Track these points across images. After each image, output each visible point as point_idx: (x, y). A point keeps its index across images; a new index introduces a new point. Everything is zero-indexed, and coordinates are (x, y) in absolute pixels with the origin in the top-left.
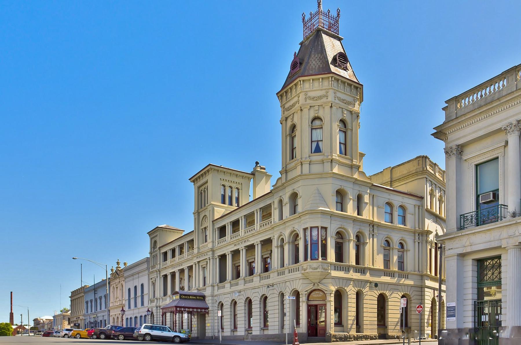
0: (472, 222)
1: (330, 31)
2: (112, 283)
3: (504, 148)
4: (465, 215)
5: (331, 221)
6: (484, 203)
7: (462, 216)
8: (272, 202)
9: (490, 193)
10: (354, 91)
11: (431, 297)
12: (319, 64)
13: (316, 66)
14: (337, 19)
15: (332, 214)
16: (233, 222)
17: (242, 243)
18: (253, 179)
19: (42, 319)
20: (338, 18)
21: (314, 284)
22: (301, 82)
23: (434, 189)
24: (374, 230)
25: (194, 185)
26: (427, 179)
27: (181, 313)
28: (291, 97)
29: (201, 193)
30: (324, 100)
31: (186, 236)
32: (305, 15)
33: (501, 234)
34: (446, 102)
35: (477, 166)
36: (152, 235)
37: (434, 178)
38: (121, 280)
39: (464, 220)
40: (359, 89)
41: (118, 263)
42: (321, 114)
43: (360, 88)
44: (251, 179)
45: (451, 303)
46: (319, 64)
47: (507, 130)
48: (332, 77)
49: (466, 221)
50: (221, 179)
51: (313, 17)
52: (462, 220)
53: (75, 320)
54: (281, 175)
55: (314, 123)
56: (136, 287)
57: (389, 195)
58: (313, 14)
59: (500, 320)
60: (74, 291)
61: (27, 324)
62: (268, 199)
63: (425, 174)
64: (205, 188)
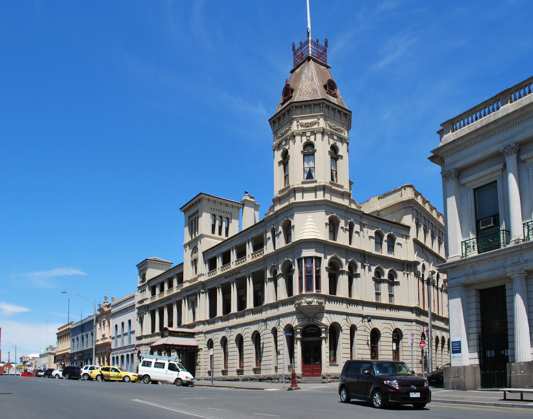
0: (474, 249)
1: (319, 59)
2: (99, 318)
3: (502, 171)
5: (325, 251)
6: (484, 229)
7: (463, 243)
8: (231, 248)
9: (491, 218)
10: (343, 118)
11: (421, 332)
12: (310, 91)
13: (307, 92)
14: (325, 48)
15: (326, 244)
16: (161, 283)
17: (233, 275)
18: (242, 208)
19: (29, 357)
20: (325, 47)
21: (309, 319)
22: (293, 108)
23: (419, 217)
24: (366, 260)
25: (185, 214)
26: (413, 208)
27: (169, 352)
28: (283, 123)
29: (192, 223)
30: (316, 126)
31: (175, 269)
32: (295, 45)
33: (505, 261)
34: (441, 125)
35: (475, 190)
36: (141, 268)
37: (419, 207)
38: (109, 316)
40: (348, 116)
41: (106, 298)
42: (312, 139)
43: (349, 115)
44: (240, 209)
45: (456, 338)
46: (310, 91)
47: (505, 152)
49: (531, 230)
50: (211, 208)
51: (303, 45)
52: (464, 247)
53: (61, 359)
54: (274, 203)
55: (306, 149)
56: (123, 323)
57: (379, 224)
58: (302, 43)
59: (506, 355)
60: (62, 326)
61: (14, 362)
62: (260, 228)
63: (411, 203)
64: (195, 218)
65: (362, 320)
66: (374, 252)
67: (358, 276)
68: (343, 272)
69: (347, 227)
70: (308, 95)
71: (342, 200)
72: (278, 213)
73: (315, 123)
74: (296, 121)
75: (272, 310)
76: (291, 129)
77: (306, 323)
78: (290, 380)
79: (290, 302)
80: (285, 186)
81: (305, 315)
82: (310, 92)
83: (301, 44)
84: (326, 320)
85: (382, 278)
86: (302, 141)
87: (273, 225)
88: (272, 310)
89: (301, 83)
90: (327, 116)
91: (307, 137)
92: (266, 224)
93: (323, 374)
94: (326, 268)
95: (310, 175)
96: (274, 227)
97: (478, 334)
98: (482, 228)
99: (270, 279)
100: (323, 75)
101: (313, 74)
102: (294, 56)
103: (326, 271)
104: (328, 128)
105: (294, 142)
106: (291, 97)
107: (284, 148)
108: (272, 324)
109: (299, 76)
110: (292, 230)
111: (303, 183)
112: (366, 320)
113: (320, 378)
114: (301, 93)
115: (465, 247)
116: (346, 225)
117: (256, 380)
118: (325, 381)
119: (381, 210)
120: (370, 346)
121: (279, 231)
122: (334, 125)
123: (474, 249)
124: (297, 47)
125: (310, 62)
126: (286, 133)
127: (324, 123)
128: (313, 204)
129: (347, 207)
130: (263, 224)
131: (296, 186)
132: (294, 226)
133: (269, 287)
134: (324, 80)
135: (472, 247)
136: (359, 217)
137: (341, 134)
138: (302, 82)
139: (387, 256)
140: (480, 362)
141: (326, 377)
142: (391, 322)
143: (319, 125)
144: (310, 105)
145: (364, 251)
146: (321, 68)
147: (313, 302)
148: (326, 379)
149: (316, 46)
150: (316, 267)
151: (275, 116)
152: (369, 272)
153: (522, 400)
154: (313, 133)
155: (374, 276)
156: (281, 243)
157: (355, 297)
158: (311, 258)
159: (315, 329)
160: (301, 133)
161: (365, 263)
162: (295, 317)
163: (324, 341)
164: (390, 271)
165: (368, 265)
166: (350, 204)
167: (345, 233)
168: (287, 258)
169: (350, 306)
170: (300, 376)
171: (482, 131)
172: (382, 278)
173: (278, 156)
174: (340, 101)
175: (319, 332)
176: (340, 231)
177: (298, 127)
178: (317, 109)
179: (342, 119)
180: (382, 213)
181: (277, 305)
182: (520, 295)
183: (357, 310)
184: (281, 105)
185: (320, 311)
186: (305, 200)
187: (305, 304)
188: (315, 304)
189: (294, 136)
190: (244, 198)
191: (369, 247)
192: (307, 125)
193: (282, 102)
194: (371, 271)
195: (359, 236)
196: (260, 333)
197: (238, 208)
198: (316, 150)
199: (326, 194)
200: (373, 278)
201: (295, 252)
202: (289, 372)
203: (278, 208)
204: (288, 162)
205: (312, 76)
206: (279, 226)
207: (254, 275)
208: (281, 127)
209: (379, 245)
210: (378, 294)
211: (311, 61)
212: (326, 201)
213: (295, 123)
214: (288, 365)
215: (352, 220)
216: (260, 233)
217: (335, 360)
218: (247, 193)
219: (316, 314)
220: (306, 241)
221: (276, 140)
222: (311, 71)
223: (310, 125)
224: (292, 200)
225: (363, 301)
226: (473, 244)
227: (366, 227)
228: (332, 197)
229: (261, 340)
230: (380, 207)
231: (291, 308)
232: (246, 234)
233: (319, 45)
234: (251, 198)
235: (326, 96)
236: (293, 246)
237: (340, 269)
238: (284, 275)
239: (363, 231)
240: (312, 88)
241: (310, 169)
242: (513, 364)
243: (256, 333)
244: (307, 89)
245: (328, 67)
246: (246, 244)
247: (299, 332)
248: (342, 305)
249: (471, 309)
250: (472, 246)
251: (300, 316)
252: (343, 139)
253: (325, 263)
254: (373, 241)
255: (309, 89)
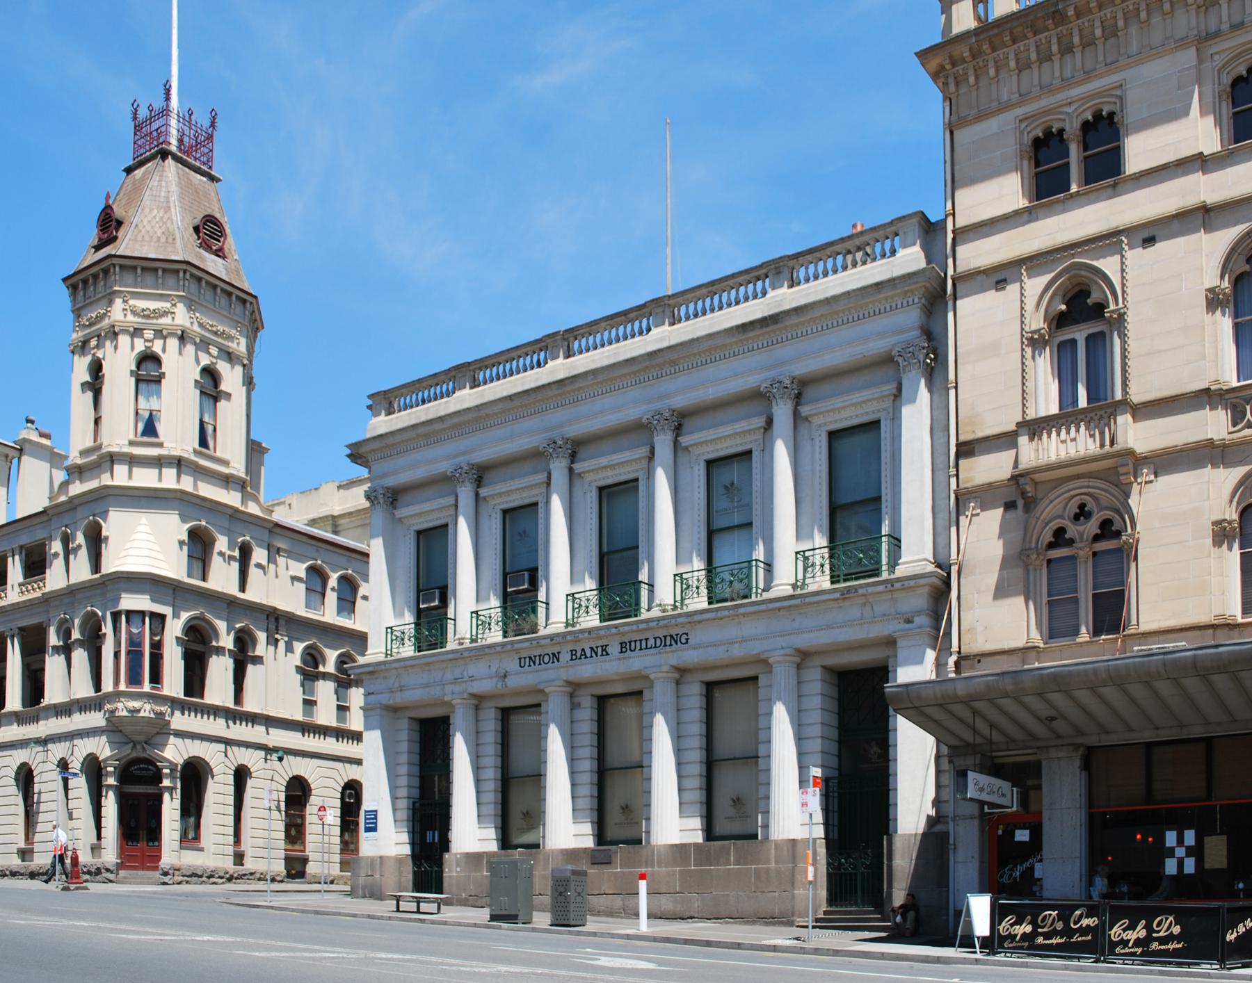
0: (823, 572)
4: (576, 596)
10: (238, 308)
13: (152, 237)
30: (166, 320)
35: (505, 512)
39: (573, 607)
42: (157, 347)
43: (251, 303)
46: (159, 235)
48: (185, 271)
52: (800, 564)
55: (143, 365)
57: (318, 551)
65: (266, 756)
66: (302, 612)
67: (258, 660)
68: (220, 651)
69: (234, 551)
70: (153, 244)
71: (226, 491)
72: (76, 502)
73: (166, 313)
74: (121, 300)
75: (59, 717)
76: (109, 314)
77: (128, 755)
78: (91, 875)
79: (95, 705)
80: (95, 442)
81: (126, 736)
82: (159, 238)
83: (151, 111)
84: (174, 752)
85: (321, 669)
86: (133, 348)
87: (66, 526)
88: (59, 717)
89: (139, 210)
90: (196, 302)
91: (146, 341)
92: (50, 520)
93: (162, 866)
94: (177, 638)
95: (150, 429)
96: (67, 533)
97: (411, 800)
98: (425, 606)
99: (57, 649)
100: (198, 199)
101: (171, 194)
102: (135, 134)
103: (178, 645)
104: (196, 328)
105: (116, 347)
106: (115, 238)
107: (94, 355)
108: (58, 751)
109: (139, 188)
110: (103, 545)
111: (131, 443)
112: (275, 757)
113: (157, 874)
114: (136, 236)
115: (682, 587)
116: (231, 547)
117: (22, 874)
118: (166, 881)
119: (342, 516)
120: (283, 813)
121: (77, 542)
122: (211, 323)
123: (823, 572)
124: (143, 113)
125: (167, 161)
126: (100, 322)
127: (187, 316)
128: (151, 494)
129: (236, 510)
130: (44, 518)
131: (115, 449)
132: (107, 538)
133: (53, 665)
134: (198, 210)
135: (818, 567)
136: (267, 532)
137: (230, 344)
138: (143, 210)
139: (336, 623)
140: (413, 850)
141: (170, 871)
142: (339, 765)
143: (173, 318)
144: (156, 270)
145: (275, 609)
146: (194, 180)
147: (142, 711)
148: (169, 877)
149: (187, 123)
150: (152, 633)
151: (75, 274)
152: (288, 654)
153: (418, 912)
154: (159, 333)
155: (299, 663)
156: (81, 571)
157: (251, 704)
158: (142, 614)
159: (150, 767)
160: (131, 329)
161: (277, 633)
162: (104, 738)
163: (166, 796)
164: (340, 655)
165: (286, 639)
166: (243, 502)
167: (229, 564)
168: (92, 606)
169: (235, 724)
170: (112, 868)
171: (422, 430)
172: (321, 669)
173: (81, 367)
174: (233, 267)
175: (158, 777)
176: (216, 562)
177: (125, 315)
178: (171, 280)
179: (234, 309)
180: (342, 521)
181: (70, 710)
182: (557, 726)
183: (256, 733)
184: (93, 250)
185: (161, 730)
186: (135, 483)
187: (125, 713)
188: (146, 714)
189: (116, 334)
190: (24, 434)
191: (292, 600)
192: (146, 314)
193: (96, 243)
194: (292, 652)
195: (265, 574)
196: (33, 768)
197: (7, 456)
198: (164, 373)
199: (183, 476)
200: (297, 667)
201: (108, 596)
202: (93, 858)
203: (77, 488)
204: (100, 388)
205: (167, 198)
206: (77, 530)
207: (25, 634)
208: (91, 304)
209: (318, 597)
210: (309, 704)
211: (170, 161)
212: (181, 491)
213: (118, 303)
214: (92, 844)
215: (248, 538)
216: (37, 539)
217: (197, 837)
218: (32, 422)
219: (152, 737)
220: (130, 576)
221: (78, 331)
222: (167, 187)
223: (152, 315)
224: (106, 480)
225: (268, 716)
226: (696, 582)
227: (284, 556)
228: (199, 483)
229: (36, 786)
230: (341, 508)
231: (96, 719)
232: (9, 534)
233: (193, 122)
234: (42, 435)
235: (198, 252)
236: (103, 583)
237: (214, 643)
238: (86, 643)
239: (275, 563)
240: (164, 228)
241: (151, 414)
242: (447, 856)
243: (26, 768)
244: (153, 227)
245: (213, 179)
246: (7, 558)
247: (111, 772)
248: (215, 720)
249: (691, 736)
250: (818, 563)
251: (117, 738)
252: (233, 356)
253: (175, 628)
254: (302, 587)
255: (156, 230)
